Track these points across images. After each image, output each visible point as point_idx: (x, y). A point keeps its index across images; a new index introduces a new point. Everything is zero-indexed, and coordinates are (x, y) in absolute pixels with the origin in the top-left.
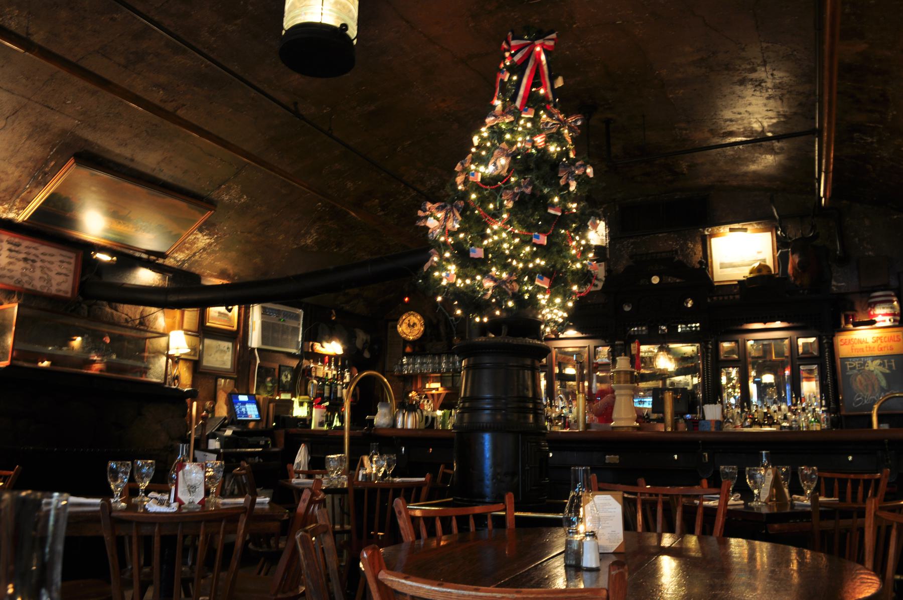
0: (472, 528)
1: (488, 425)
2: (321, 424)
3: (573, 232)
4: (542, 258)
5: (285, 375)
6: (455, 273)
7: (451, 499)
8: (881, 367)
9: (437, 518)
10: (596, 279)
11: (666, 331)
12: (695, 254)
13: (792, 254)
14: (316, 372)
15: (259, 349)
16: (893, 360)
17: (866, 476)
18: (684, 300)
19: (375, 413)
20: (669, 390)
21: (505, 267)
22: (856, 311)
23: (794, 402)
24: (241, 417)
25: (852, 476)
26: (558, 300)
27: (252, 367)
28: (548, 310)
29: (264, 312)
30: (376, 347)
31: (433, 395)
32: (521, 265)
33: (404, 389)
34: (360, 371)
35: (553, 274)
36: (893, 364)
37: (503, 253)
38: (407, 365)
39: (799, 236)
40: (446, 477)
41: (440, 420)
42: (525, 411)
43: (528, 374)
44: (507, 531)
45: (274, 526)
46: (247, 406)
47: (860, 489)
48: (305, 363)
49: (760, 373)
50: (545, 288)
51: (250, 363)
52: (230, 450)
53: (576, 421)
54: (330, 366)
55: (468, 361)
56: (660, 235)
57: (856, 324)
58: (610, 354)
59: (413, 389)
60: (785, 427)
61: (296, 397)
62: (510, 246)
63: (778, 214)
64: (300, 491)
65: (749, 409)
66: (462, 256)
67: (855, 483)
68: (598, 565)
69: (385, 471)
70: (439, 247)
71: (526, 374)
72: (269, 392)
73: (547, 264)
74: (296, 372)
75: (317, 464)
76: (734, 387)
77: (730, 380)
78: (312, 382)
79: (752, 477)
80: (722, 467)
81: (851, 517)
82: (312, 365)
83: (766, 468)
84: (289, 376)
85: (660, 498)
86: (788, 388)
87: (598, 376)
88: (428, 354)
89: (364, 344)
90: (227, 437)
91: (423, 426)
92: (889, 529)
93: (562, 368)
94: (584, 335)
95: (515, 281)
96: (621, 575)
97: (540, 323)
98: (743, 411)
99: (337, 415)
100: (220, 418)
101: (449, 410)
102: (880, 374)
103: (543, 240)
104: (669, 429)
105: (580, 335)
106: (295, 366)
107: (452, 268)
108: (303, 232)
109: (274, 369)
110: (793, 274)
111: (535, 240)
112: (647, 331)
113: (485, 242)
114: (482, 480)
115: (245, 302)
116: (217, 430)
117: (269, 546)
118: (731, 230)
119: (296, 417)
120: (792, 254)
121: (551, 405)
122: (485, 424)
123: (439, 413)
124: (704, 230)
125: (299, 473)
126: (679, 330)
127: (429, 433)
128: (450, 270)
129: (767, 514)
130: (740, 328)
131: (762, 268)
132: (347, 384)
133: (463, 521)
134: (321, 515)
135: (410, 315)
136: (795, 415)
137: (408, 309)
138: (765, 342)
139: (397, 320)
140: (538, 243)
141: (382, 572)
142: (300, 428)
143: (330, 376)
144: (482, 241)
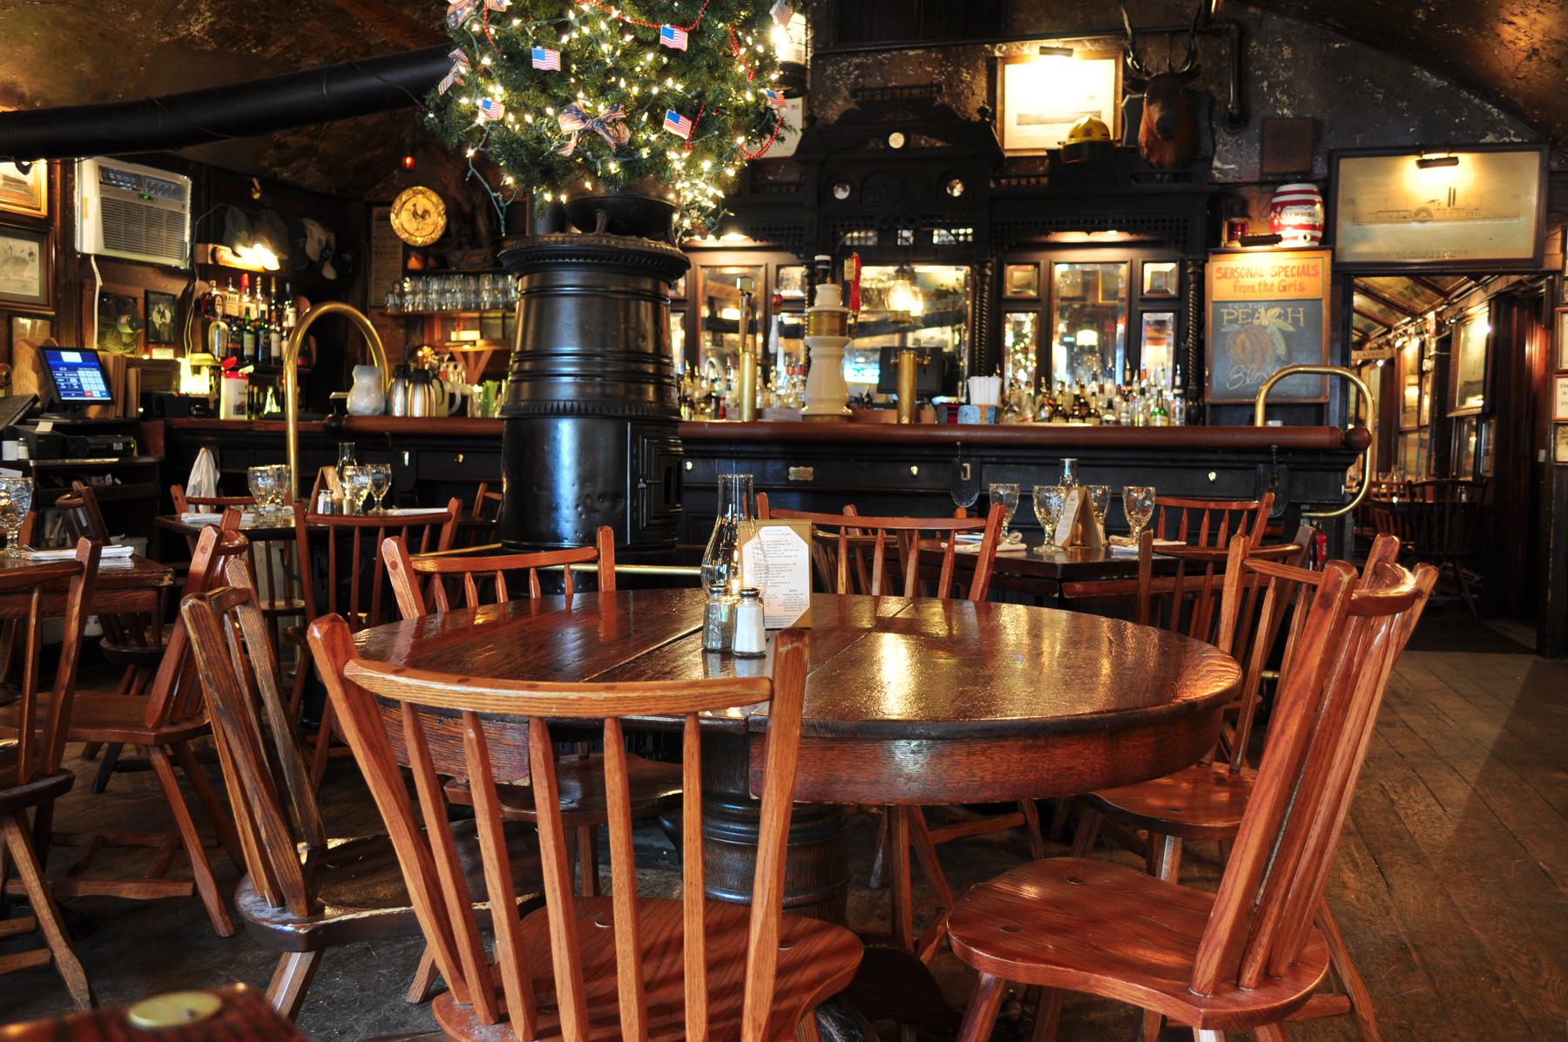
0: (534, 591)
1: (569, 404)
2: (239, 409)
3: (741, 27)
4: (680, 76)
5: (159, 312)
6: (503, 102)
7: (500, 545)
8: (1281, 321)
9: (468, 575)
10: (782, 125)
11: (911, 240)
12: (973, 94)
13: (1149, 104)
14: (224, 306)
15: (97, 257)
16: (1301, 309)
17: (1235, 506)
18: (946, 181)
19: (347, 385)
20: (909, 349)
21: (603, 91)
22: (1249, 217)
23: (1128, 378)
24: (70, 395)
25: (1212, 505)
26: (706, 165)
27: (86, 293)
28: (687, 184)
29: (105, 177)
30: (348, 257)
31: (465, 355)
32: (635, 91)
33: (407, 343)
34: (315, 303)
35: (698, 111)
36: (1301, 316)
37: (601, 63)
38: (414, 296)
39: (1165, 69)
40: (489, 506)
41: (478, 401)
42: (640, 378)
43: (646, 308)
44: (601, 596)
45: (144, 597)
46: (81, 373)
47: (1224, 526)
48: (200, 285)
49: (1073, 328)
50: (682, 139)
51: (82, 286)
52: (50, 462)
53: (738, 405)
54: (253, 294)
55: (530, 281)
56: (911, 53)
57: (1247, 242)
58: (806, 280)
59: (426, 342)
60: (1107, 421)
61: (184, 356)
62: (615, 49)
63: (1130, 25)
64: (196, 534)
65: (1049, 388)
66: (515, 62)
67: (1216, 516)
68: (763, 648)
69: (370, 496)
70: (471, 46)
71: (643, 309)
72: (126, 345)
73: (686, 90)
74: (180, 305)
75: (233, 487)
76: (1025, 351)
77: (1019, 336)
78: (218, 326)
79: (1043, 503)
80: (993, 486)
81: (1203, 573)
82: (215, 292)
83: (1069, 488)
84: (168, 314)
85: (880, 538)
86: (1120, 354)
87: (781, 324)
88: (454, 273)
89: (323, 251)
90: (42, 436)
91: (444, 411)
92: (1262, 591)
93: (717, 308)
94: (758, 244)
95: (624, 121)
96: (797, 652)
97: (671, 209)
98: (1038, 392)
99: (271, 391)
100: (23, 398)
101: (495, 380)
102: (1278, 334)
103: (679, 40)
104: (905, 420)
105: (750, 243)
106: (179, 294)
107: (497, 91)
108: (181, 7)
109: (135, 300)
110: (1147, 143)
111: (664, 40)
112: (875, 239)
113: (565, 39)
114: (554, 508)
115: (63, 153)
116: (18, 423)
117: (142, 642)
118: (1044, 51)
119: (186, 397)
120: (1149, 104)
121: (692, 376)
122: (562, 404)
123: (477, 389)
124: (994, 47)
125: (196, 502)
126: (936, 240)
127: (459, 426)
128: (491, 95)
129: (1064, 566)
130: (1044, 239)
131: (1094, 126)
132: (290, 330)
133: (517, 580)
134: (235, 574)
135: (415, 193)
136: (1127, 400)
137: (411, 179)
138: (1088, 268)
139: (390, 204)
140: (671, 46)
141: (351, 663)
142: (196, 416)
143: (254, 315)
144: (559, 39)
